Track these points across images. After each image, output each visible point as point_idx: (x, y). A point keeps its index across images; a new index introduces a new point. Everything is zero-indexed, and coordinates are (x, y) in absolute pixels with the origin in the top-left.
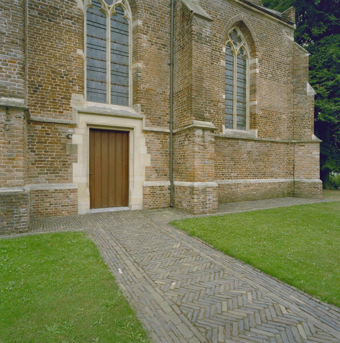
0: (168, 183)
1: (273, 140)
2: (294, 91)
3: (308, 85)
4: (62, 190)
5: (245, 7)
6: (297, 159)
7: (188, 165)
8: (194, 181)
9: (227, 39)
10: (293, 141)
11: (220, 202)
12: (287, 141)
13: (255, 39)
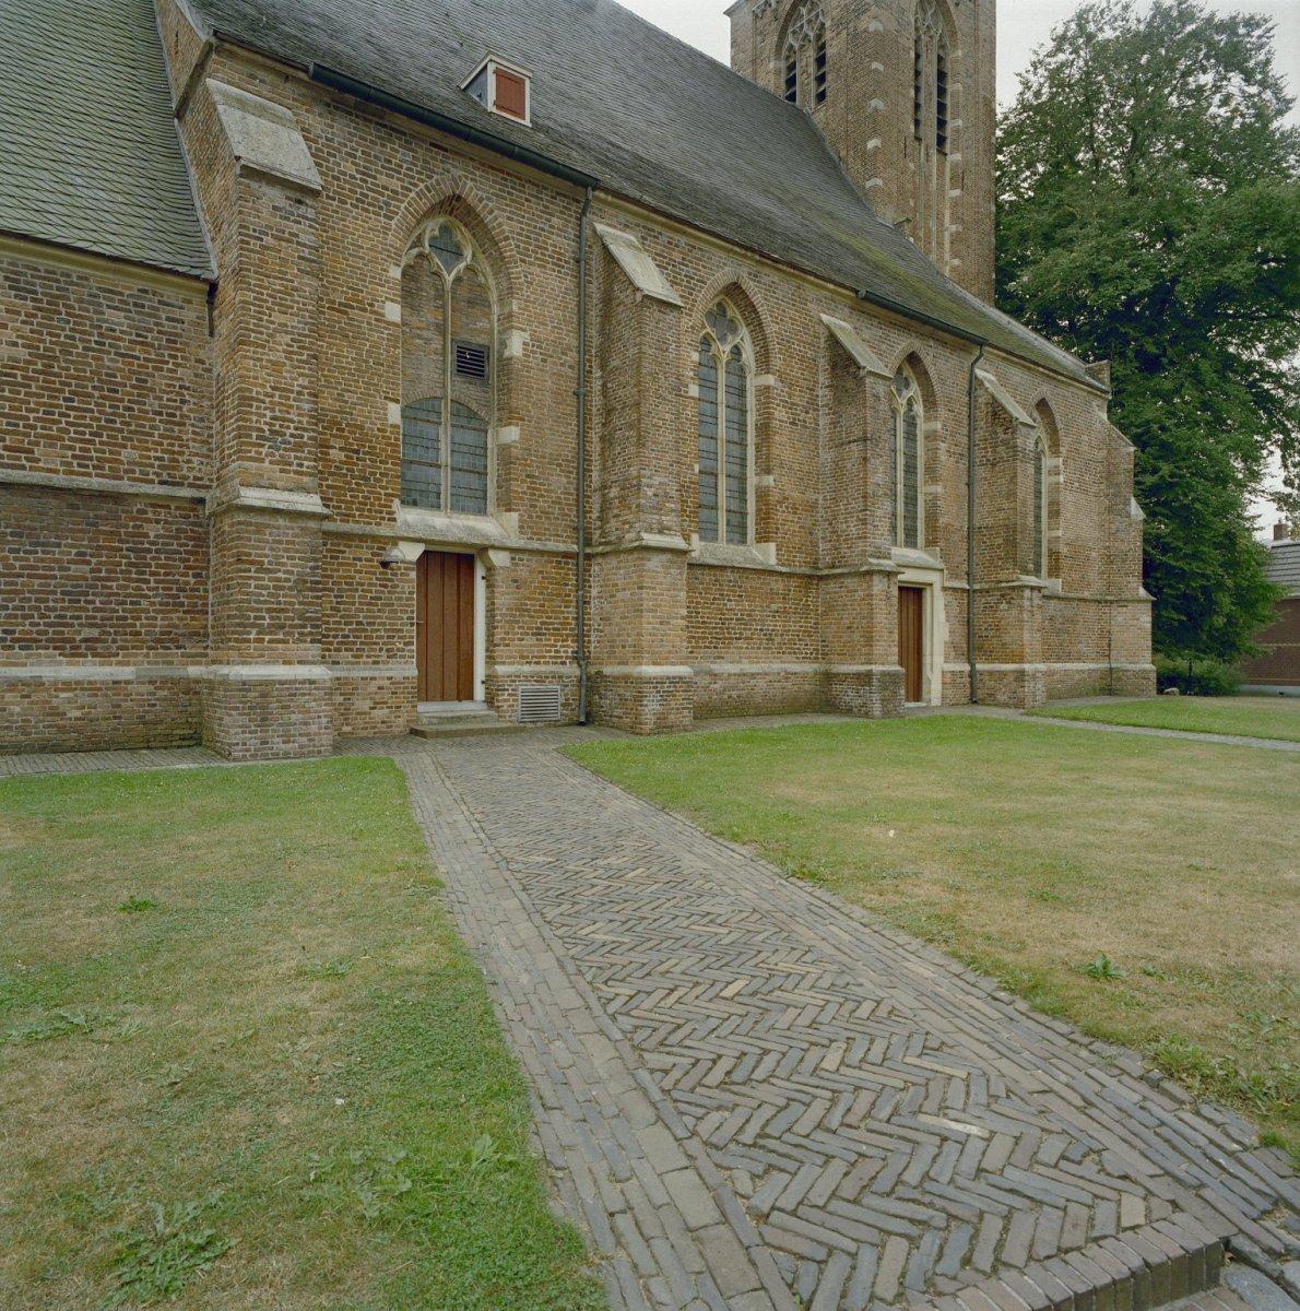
0: (967, 668)
1: (1080, 595)
2: (1110, 510)
3: (1133, 501)
4: (96, 682)
5: (1048, 376)
6: (1115, 629)
7: (1007, 639)
8: (1021, 661)
9: (704, 327)
10: (1109, 598)
11: (1050, 696)
12: (1099, 597)
13: (1060, 426)
